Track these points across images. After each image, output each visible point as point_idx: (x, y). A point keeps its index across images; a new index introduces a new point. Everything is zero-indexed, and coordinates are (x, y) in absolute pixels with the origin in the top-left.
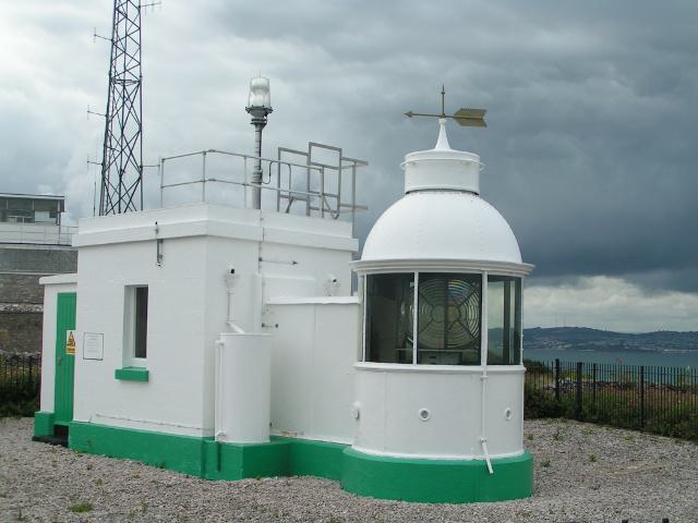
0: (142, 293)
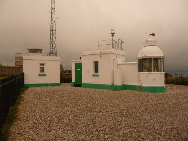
0: (96, 64)
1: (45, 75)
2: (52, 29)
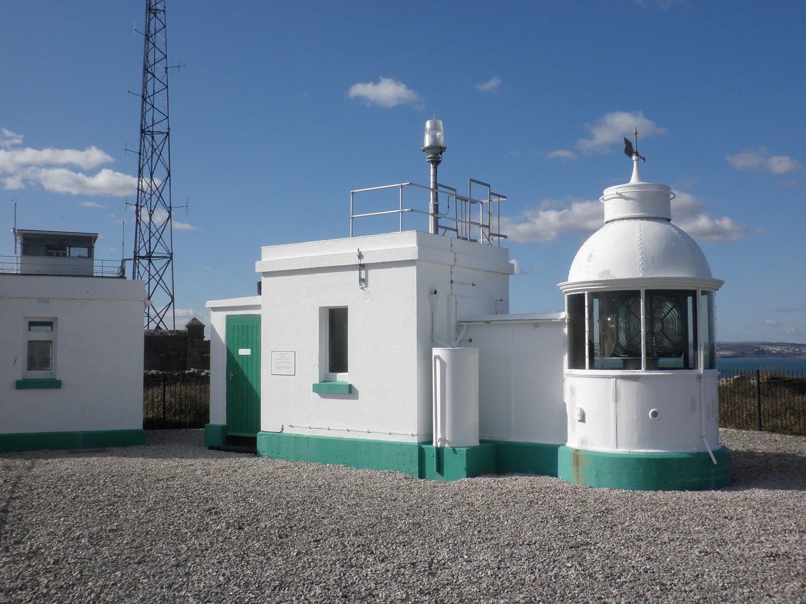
0: (336, 322)
1: (350, 392)
2: (149, 123)
